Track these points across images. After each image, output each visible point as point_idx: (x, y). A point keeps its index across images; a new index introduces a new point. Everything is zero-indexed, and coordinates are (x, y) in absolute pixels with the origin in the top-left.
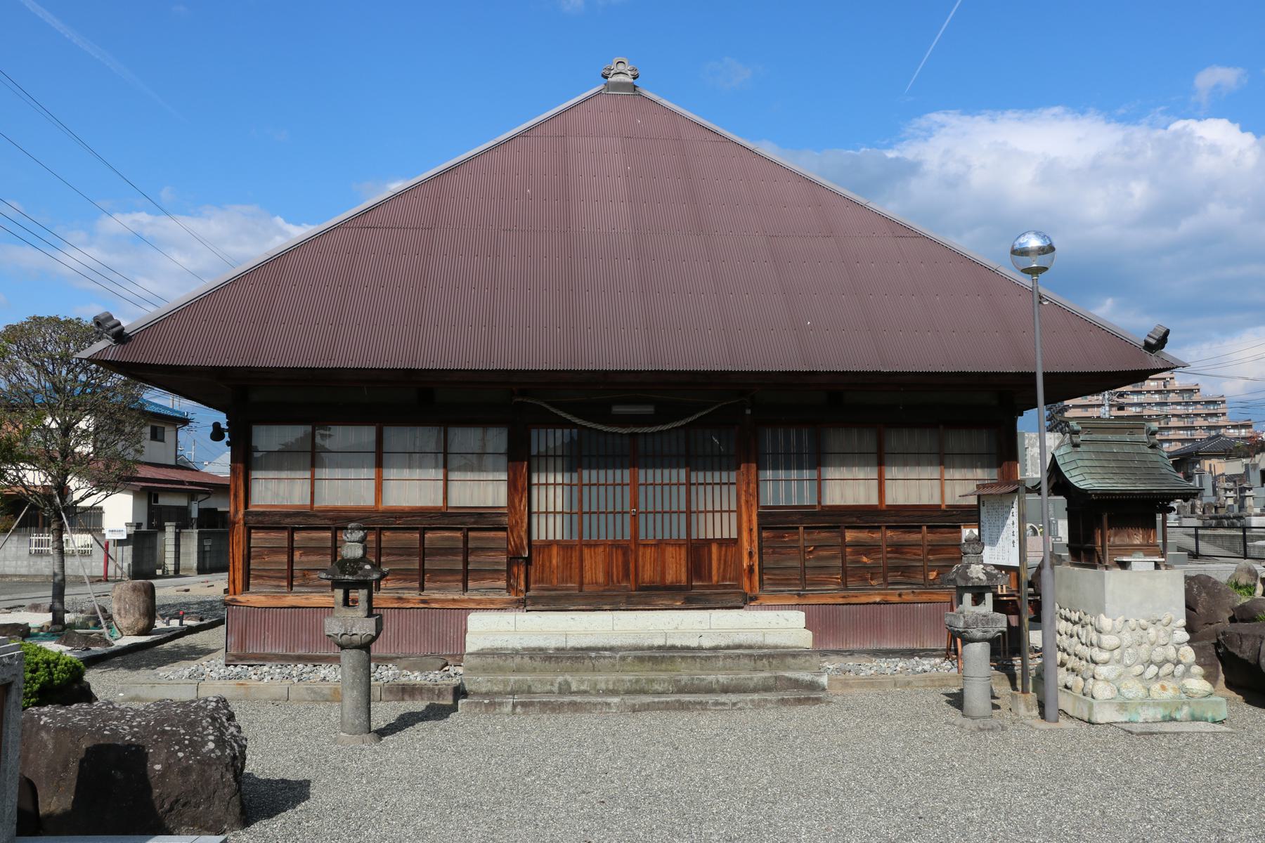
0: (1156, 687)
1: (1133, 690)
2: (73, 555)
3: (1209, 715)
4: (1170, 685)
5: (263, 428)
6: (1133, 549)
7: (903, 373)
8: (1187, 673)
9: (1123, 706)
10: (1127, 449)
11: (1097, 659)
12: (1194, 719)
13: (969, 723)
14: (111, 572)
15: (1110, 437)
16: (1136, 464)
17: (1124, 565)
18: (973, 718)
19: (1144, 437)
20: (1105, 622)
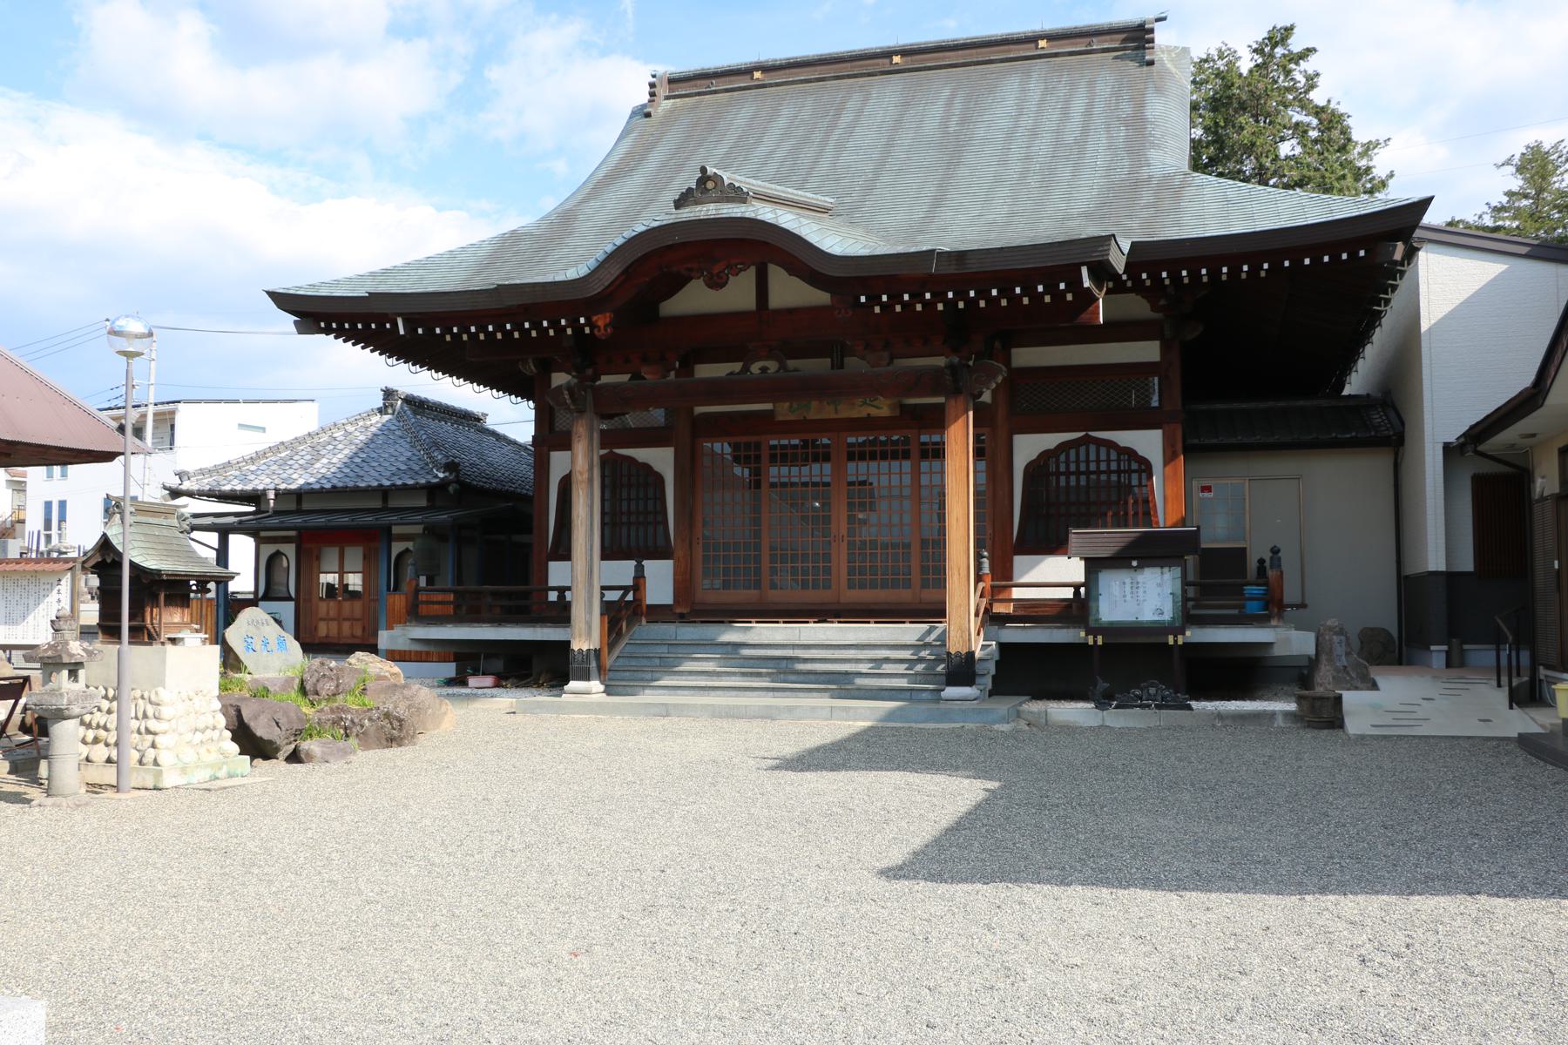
0: (203, 750)
1: (189, 756)
2: (916, 473)
3: (239, 772)
4: (213, 748)
5: (532, 414)
6: (180, 626)
7: (1478, 424)
8: (221, 738)
9: (184, 770)
10: (165, 532)
11: (152, 728)
12: (231, 776)
13: (64, 802)
14: (213, 538)
15: (151, 520)
16: (175, 547)
17: (173, 641)
18: (65, 796)
19: (175, 522)
20: (164, 694)
